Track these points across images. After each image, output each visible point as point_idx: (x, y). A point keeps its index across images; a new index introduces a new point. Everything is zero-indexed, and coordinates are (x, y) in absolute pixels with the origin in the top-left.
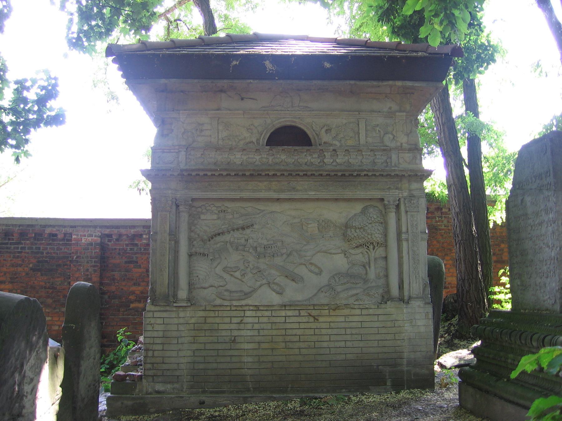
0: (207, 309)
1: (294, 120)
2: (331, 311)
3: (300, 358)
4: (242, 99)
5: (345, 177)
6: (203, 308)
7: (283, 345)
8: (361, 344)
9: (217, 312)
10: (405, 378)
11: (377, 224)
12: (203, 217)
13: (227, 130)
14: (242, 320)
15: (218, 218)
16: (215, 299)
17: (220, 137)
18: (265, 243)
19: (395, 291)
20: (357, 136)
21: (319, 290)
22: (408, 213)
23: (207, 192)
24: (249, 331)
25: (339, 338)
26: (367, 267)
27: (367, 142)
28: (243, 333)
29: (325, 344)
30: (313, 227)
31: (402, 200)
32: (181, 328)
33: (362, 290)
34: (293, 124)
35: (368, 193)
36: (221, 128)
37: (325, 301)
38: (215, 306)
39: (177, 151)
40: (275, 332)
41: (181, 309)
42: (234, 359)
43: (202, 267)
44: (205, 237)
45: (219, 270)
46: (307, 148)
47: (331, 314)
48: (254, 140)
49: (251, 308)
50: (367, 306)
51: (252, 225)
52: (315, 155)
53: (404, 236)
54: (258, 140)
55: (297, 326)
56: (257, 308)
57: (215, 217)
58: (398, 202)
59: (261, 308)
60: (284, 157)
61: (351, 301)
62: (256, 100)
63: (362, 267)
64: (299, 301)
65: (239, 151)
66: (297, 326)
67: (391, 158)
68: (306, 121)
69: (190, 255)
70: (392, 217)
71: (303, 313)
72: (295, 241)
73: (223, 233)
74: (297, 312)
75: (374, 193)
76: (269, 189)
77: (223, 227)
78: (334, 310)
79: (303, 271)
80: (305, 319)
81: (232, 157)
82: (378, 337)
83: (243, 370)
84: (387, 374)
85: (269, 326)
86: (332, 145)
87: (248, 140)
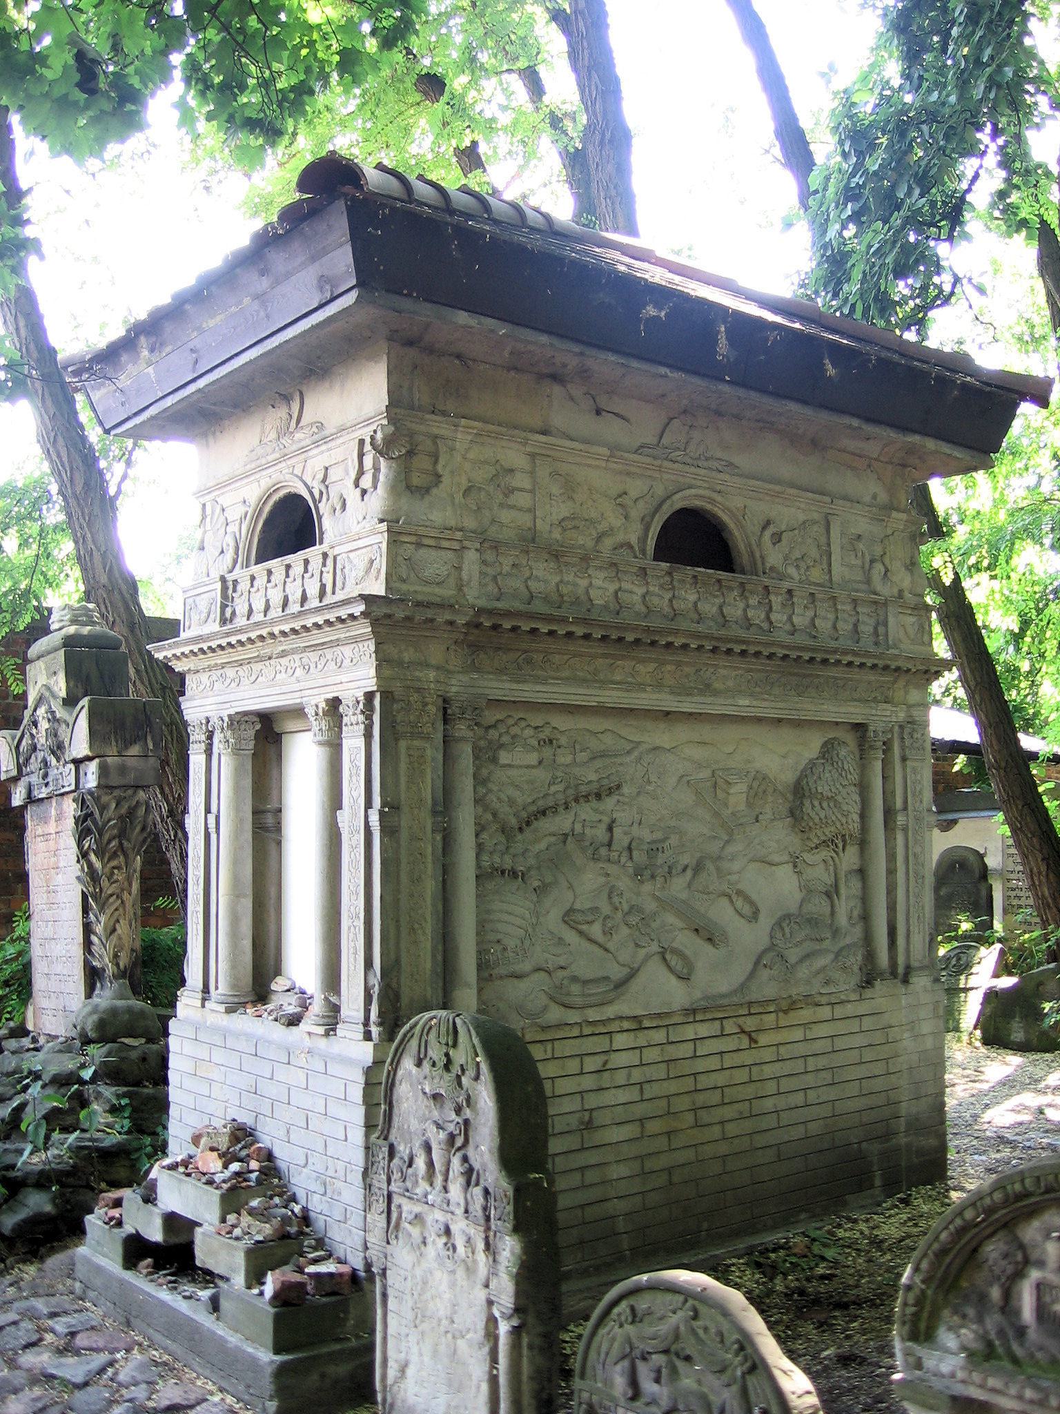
2: (781, 1014)
3: (723, 1148)
4: (598, 412)
5: (804, 665)
8: (832, 1093)
9: (549, 1046)
10: (903, 1164)
12: (504, 758)
13: (571, 498)
14: (605, 1063)
16: (545, 1008)
21: (757, 963)
22: (908, 762)
23: (525, 681)
24: (620, 1091)
25: (794, 1083)
28: (609, 1098)
29: (769, 1104)
30: (738, 795)
33: (832, 956)
34: (709, 507)
35: (843, 710)
37: (770, 991)
38: (544, 1028)
39: (456, 546)
42: (591, 1176)
43: (514, 909)
44: (513, 822)
45: (553, 919)
46: (723, 575)
47: (782, 1023)
48: (634, 540)
50: (843, 997)
51: (619, 787)
53: (900, 819)
56: (638, 1024)
57: (533, 758)
59: (646, 1023)
60: (692, 595)
61: (816, 987)
62: (628, 421)
63: (824, 897)
64: (723, 996)
65: (601, 568)
67: (886, 624)
68: (739, 507)
71: (730, 1027)
72: (705, 831)
73: (554, 809)
74: (717, 1024)
75: (852, 710)
76: (659, 686)
77: (553, 789)
78: (785, 1012)
79: (723, 914)
80: (731, 1043)
82: (862, 1071)
83: (608, 1205)
84: (875, 1159)
85: (660, 1071)
87: (620, 537)
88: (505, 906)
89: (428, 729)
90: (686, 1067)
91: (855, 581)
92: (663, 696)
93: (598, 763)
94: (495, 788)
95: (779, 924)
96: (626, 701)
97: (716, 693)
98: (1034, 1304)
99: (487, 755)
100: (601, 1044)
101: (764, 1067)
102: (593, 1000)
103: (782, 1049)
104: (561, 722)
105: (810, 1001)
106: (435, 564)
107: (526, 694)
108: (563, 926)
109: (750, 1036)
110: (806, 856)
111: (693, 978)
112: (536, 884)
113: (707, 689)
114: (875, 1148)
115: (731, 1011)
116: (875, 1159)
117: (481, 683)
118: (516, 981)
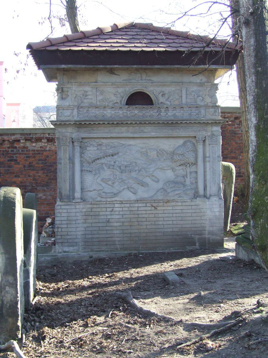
0: (92, 203)
1: (143, 88)
2: (164, 203)
3: (146, 231)
6: (90, 203)
7: (137, 223)
8: (182, 222)
9: (98, 205)
11: (192, 152)
12: (88, 149)
13: (102, 95)
14: (113, 209)
15: (98, 149)
16: (97, 198)
17: (98, 100)
18: (126, 163)
19: (201, 192)
20: (181, 98)
26: (186, 178)
27: (186, 102)
31: (207, 137)
32: (77, 214)
34: (142, 91)
36: (98, 94)
37: (160, 198)
39: (72, 109)
40: (132, 216)
41: (77, 204)
43: (89, 179)
44: (90, 161)
45: (99, 180)
46: (151, 106)
48: (119, 101)
49: (118, 202)
50: (185, 201)
52: (156, 111)
53: (207, 159)
54: (121, 101)
55: (144, 212)
56: (121, 202)
57: (96, 148)
58: (204, 139)
60: (136, 112)
61: (176, 198)
66: (144, 212)
68: (151, 90)
69: (82, 171)
70: (200, 148)
71: (148, 205)
73: (101, 158)
74: (145, 204)
77: (100, 154)
79: (148, 180)
80: (150, 208)
81: (105, 112)
84: (197, 239)
85: (128, 213)
86: (164, 104)
87: (115, 102)
88: (87, 178)
89: (68, 144)
90: (136, 212)
91: (192, 102)
92: (129, 134)
93: (113, 149)
94: (86, 155)
95: (165, 183)
97: (145, 132)
98: (35, 263)
99: (83, 148)
100: (113, 206)
101: (159, 214)
102: (109, 197)
103: (165, 211)
104: (104, 141)
105: (173, 201)
106: (67, 113)
108: (102, 182)
109: (155, 207)
110: (176, 168)
111: (137, 194)
113: (143, 132)
114: (197, 237)
115: (153, 203)
116: (197, 239)
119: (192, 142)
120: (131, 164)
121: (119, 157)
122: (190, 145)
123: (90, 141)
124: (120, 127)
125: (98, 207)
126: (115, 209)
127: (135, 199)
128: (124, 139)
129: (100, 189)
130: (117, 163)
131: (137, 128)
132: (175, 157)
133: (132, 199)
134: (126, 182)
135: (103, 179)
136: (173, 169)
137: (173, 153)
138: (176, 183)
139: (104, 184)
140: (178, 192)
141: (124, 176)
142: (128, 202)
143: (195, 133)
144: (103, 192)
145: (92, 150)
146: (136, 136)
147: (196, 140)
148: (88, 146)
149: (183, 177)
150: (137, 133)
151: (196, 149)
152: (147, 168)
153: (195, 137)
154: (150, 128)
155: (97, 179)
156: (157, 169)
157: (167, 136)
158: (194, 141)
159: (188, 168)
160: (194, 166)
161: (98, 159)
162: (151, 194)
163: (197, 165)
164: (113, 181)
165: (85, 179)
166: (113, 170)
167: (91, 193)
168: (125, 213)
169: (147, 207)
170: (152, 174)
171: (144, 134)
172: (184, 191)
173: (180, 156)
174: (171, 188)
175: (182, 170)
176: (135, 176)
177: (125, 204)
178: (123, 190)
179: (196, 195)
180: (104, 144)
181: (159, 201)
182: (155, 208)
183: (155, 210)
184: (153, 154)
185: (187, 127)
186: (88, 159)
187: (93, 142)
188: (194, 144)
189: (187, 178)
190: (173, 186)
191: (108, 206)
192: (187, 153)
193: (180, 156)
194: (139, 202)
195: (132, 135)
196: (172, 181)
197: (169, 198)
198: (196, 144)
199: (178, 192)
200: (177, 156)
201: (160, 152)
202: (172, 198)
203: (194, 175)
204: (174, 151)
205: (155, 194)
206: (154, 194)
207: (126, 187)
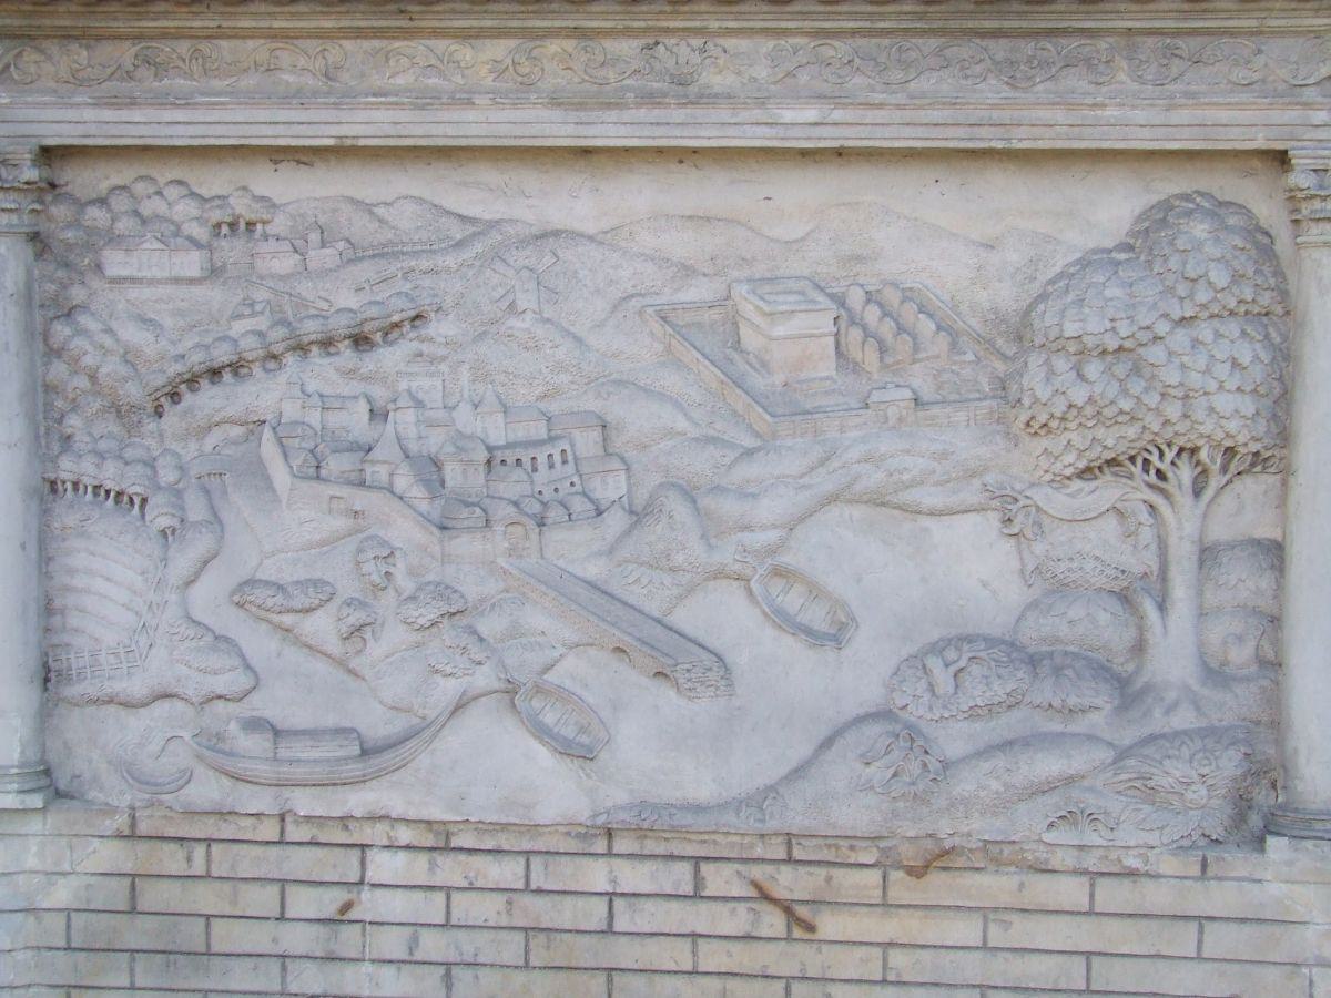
0: (143, 828)
2: (896, 875)
9: (200, 851)
11: (1232, 328)
14: (347, 907)
15: (214, 272)
16: (188, 777)
18: (496, 430)
37: (856, 815)
44: (133, 392)
45: (208, 597)
50: (1132, 862)
56: (441, 841)
57: (191, 263)
59: (464, 839)
61: (1028, 823)
64: (699, 809)
71: (720, 880)
73: (237, 367)
74: (683, 871)
77: (238, 327)
79: (726, 617)
90: (586, 951)
93: (366, 271)
96: (419, 130)
97: (707, 98)
103: (898, 959)
105: (994, 855)
107: (134, 130)
111: (604, 756)
112: (164, 522)
113: (684, 89)
117: (22, 113)
118: (123, 712)
119: (1248, 213)
120: (551, 439)
121: (433, 360)
122: (1211, 250)
123: (140, 188)
124: (436, 33)
125: (199, 867)
126: (371, 904)
127: (584, 816)
128: (488, 174)
129: (221, 684)
130: (405, 420)
131: (627, 48)
132: (1034, 380)
133: (546, 813)
134: (489, 626)
135: (251, 582)
136: (1008, 509)
137: (1020, 332)
138: (1033, 662)
139: (259, 643)
140: (1048, 765)
141: (474, 562)
142: (505, 841)
143: (1277, 116)
144: (254, 725)
145: (153, 282)
146: (608, 131)
147: (1293, 199)
148: (114, 239)
149: (1125, 598)
150: (619, 106)
151: (1284, 295)
152: (717, 489)
153: (1281, 159)
154: (768, 45)
155: (190, 583)
156: (832, 499)
157: (955, 139)
158: (1261, 200)
159: (1184, 499)
160: (1253, 488)
161: (215, 373)
162: (752, 764)
163: (1286, 473)
164: (356, 617)
165: (72, 572)
166: (361, 499)
167: (137, 722)
168: (468, 944)
169: (704, 907)
170: (772, 551)
171: (699, 113)
172: (1122, 755)
173: (1093, 369)
174: (973, 714)
175: (1111, 522)
176: (593, 570)
177: (477, 862)
178: (460, 707)
179: (1263, 797)
180: (280, 224)
181: (837, 852)
182: (798, 921)
183: (789, 939)
184: (794, 339)
185: (1186, 45)
186: (111, 368)
187: (173, 192)
188: (1261, 242)
189: (1162, 607)
190: (999, 690)
191: (301, 862)
192: (1181, 338)
193: (1093, 369)
194: (621, 845)
195: (559, 129)
196: (991, 642)
197: (944, 828)
198: (1283, 244)
199: (1048, 765)
200: (1061, 364)
201: (872, 315)
202: (981, 827)
203: (1243, 581)
204: (1027, 313)
205: (798, 772)
206: (783, 770)
207: (484, 678)
